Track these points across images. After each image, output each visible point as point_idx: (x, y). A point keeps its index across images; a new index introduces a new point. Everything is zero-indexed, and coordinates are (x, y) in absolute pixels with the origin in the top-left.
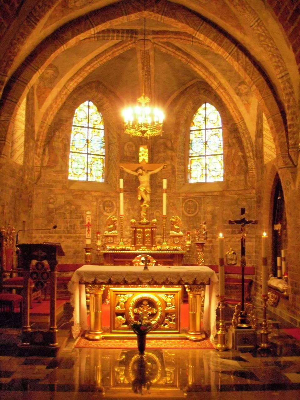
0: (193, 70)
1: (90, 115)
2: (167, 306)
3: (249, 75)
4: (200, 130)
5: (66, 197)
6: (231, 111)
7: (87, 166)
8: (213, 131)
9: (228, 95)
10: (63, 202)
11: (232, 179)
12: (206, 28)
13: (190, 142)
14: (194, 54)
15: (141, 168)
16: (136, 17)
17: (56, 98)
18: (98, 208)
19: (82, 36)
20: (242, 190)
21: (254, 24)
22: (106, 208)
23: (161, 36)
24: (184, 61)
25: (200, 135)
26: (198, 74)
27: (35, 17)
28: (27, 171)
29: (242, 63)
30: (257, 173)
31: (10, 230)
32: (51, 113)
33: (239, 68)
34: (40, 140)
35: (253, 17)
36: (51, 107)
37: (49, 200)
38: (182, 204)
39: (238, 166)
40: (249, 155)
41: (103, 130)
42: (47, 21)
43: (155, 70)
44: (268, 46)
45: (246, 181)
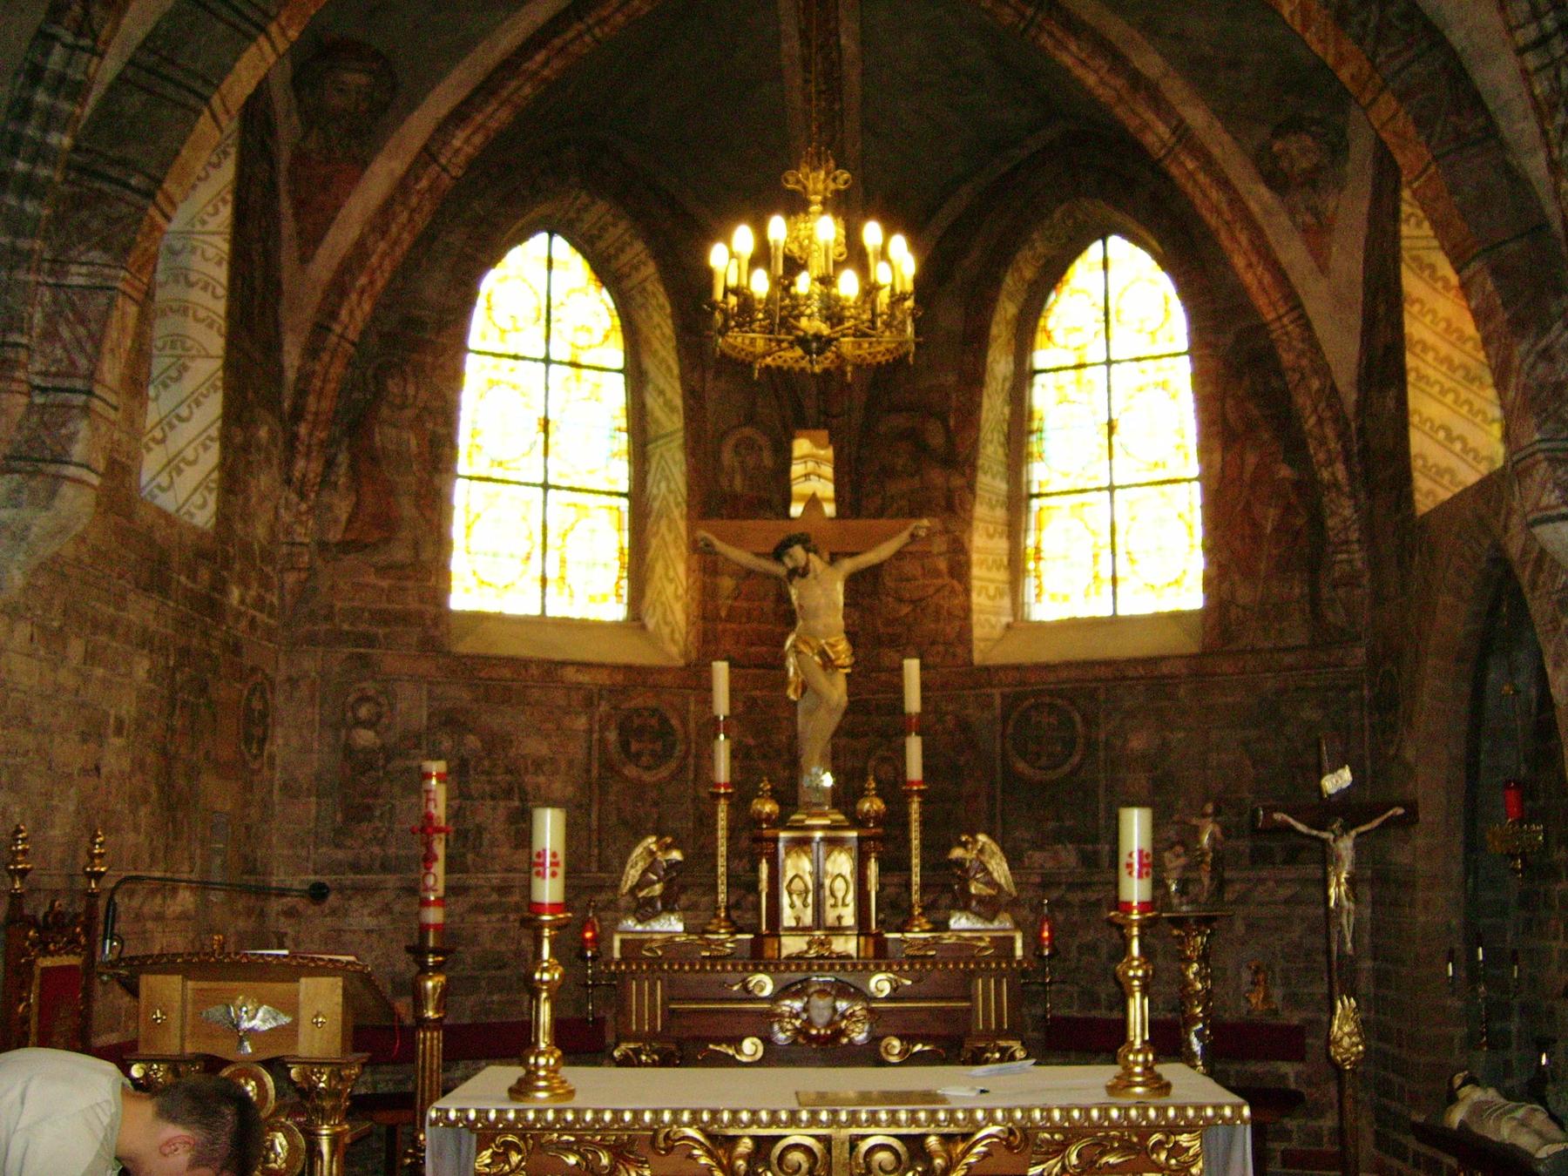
3: (1360, 41)
6: (1239, 262)
9: (1224, 183)
11: (1245, 595)
15: (804, 540)
17: (386, 210)
18: (595, 748)
22: (634, 747)
28: (237, 567)
32: (363, 280)
34: (310, 417)
36: (361, 249)
40: (1333, 474)
41: (620, 371)
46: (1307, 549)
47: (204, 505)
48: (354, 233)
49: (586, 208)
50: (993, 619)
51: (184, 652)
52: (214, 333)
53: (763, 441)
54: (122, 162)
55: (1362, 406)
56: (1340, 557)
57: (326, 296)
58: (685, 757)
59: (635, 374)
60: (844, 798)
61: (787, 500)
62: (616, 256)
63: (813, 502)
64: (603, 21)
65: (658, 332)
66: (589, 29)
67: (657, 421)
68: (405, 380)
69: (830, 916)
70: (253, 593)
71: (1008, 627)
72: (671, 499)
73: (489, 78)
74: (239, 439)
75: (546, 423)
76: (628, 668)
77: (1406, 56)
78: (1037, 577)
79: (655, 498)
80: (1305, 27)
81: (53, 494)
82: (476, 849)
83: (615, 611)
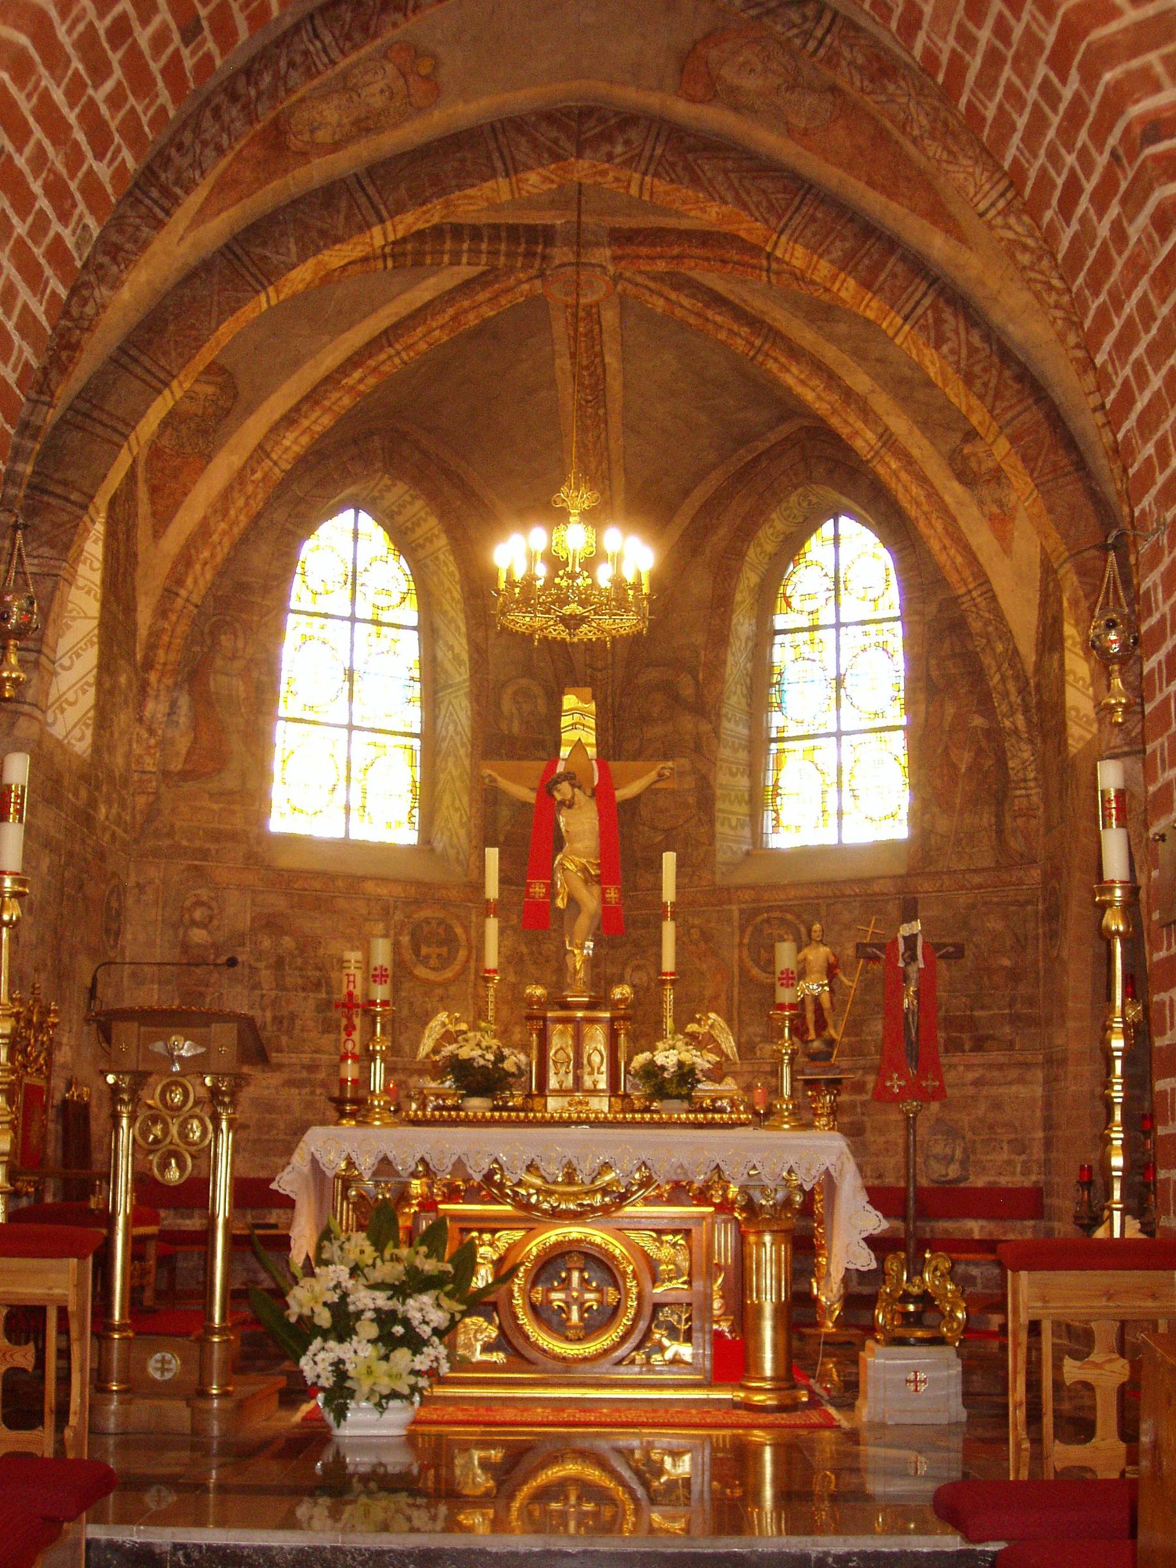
0: (776, 383)
1: (359, 569)
2: (655, 1280)
3: (981, 397)
4: (813, 628)
5: (260, 898)
6: (935, 546)
7: (348, 778)
8: (865, 634)
9: (923, 480)
10: (244, 922)
11: (943, 824)
12: (813, 219)
13: (775, 678)
14: (780, 317)
16: (546, 179)
17: (226, 495)
19: (334, 257)
20: (983, 870)
21: (993, 205)
22: (424, 950)
23: (644, 251)
24: (740, 345)
25: (817, 647)
26: (799, 399)
27: (166, 192)
28: (105, 789)
29: (952, 352)
30: (1046, 799)
31: (41, 1013)
32: (206, 554)
33: (943, 373)
34: (159, 667)
35: (989, 179)
36: (204, 530)
37: (189, 910)
38: (742, 937)
39: (970, 769)
41: (414, 628)
42: (208, 199)
43: (625, 386)
44: (1051, 288)
45: (1000, 832)
46: (996, 788)
47: (81, 739)
48: (198, 515)
49: (388, 489)
50: (735, 847)
51: (70, 854)
52: (91, 598)
53: (537, 690)
54: (65, 483)
55: (1039, 667)
56: (1018, 792)
57: (175, 565)
58: (467, 961)
59: (428, 631)
60: (600, 983)
61: (557, 744)
62: (413, 530)
63: (579, 746)
64: (410, 347)
65: (448, 596)
66: (398, 353)
67: (446, 672)
68: (236, 636)
69: (588, 1082)
70: (114, 811)
71: (748, 853)
72: (457, 739)
73: (314, 390)
74: (107, 686)
75: (350, 674)
76: (419, 883)
77: (1018, 408)
78: (776, 811)
79: (444, 739)
80: (946, 385)
81: (12, 725)
82: (289, 1032)
83: (408, 836)
